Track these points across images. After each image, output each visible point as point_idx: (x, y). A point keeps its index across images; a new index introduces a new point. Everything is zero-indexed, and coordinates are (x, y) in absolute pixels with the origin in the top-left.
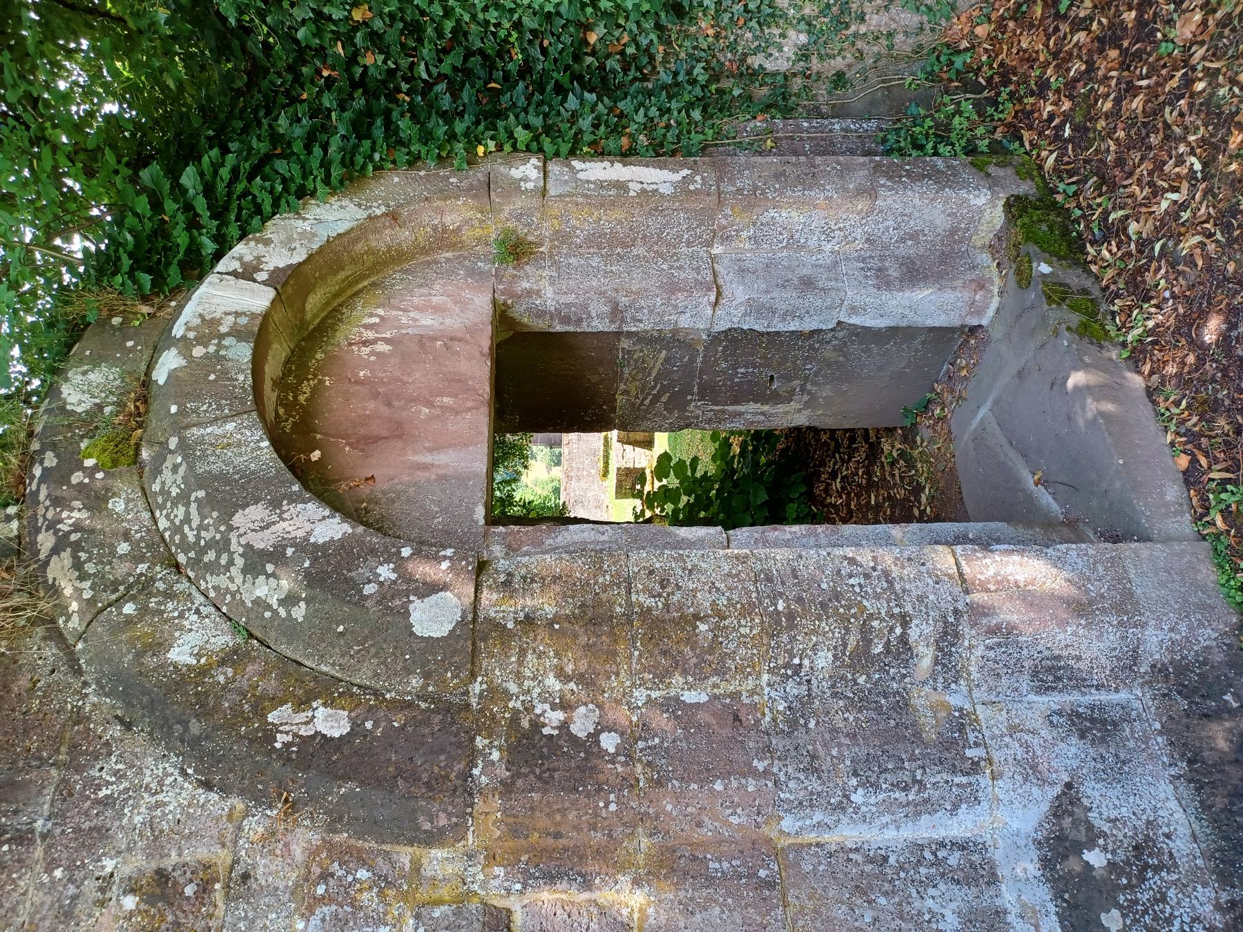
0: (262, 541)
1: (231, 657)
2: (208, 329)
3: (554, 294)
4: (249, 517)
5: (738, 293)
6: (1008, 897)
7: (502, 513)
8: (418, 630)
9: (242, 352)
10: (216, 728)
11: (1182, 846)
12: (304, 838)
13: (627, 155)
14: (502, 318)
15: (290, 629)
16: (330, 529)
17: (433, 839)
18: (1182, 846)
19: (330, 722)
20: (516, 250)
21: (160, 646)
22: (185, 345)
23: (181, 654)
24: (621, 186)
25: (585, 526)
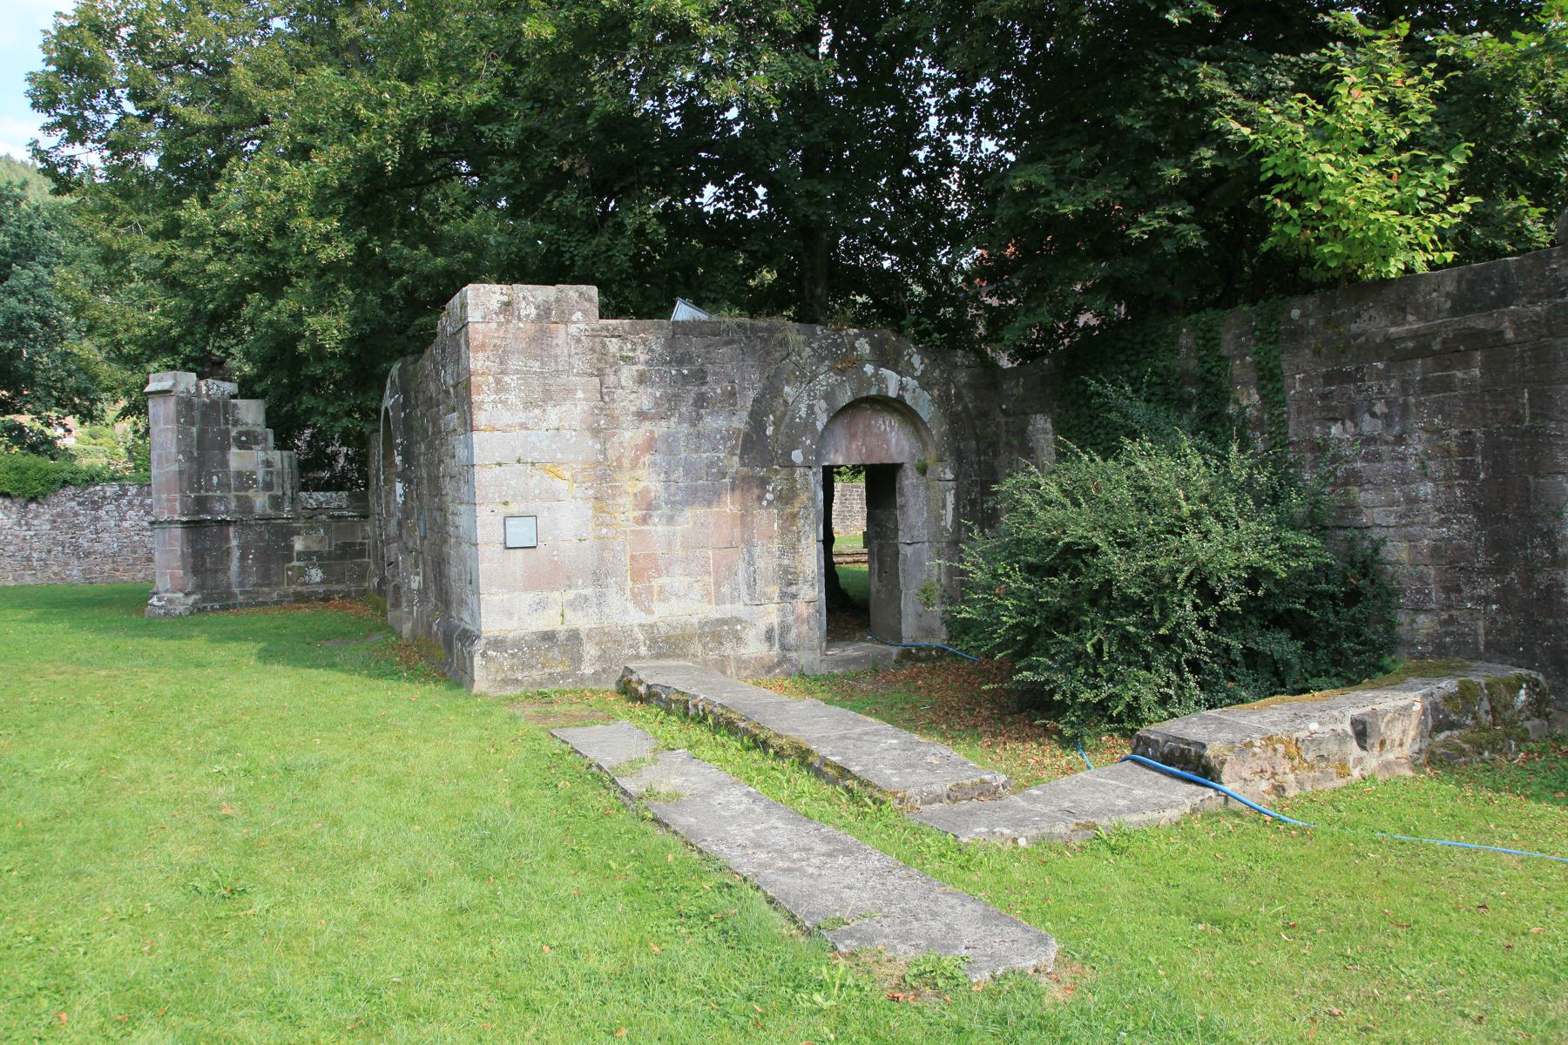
0: (816, 409)
1: (786, 402)
2: (881, 380)
3: (909, 481)
4: (823, 404)
5: (908, 550)
6: (728, 606)
7: (829, 475)
8: (595, 289)
9: (873, 392)
10: (1120, 812)
11: (742, 651)
12: (742, 426)
13: (956, 509)
14: (900, 466)
15: (793, 418)
16: (820, 426)
17: (741, 458)
18: (742, 651)
19: (770, 431)
20: (923, 470)
21: (788, 383)
22: (876, 375)
23: (787, 389)
24: (944, 507)
25: (821, 495)
